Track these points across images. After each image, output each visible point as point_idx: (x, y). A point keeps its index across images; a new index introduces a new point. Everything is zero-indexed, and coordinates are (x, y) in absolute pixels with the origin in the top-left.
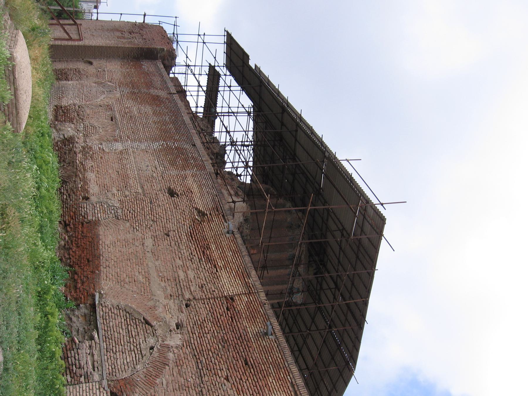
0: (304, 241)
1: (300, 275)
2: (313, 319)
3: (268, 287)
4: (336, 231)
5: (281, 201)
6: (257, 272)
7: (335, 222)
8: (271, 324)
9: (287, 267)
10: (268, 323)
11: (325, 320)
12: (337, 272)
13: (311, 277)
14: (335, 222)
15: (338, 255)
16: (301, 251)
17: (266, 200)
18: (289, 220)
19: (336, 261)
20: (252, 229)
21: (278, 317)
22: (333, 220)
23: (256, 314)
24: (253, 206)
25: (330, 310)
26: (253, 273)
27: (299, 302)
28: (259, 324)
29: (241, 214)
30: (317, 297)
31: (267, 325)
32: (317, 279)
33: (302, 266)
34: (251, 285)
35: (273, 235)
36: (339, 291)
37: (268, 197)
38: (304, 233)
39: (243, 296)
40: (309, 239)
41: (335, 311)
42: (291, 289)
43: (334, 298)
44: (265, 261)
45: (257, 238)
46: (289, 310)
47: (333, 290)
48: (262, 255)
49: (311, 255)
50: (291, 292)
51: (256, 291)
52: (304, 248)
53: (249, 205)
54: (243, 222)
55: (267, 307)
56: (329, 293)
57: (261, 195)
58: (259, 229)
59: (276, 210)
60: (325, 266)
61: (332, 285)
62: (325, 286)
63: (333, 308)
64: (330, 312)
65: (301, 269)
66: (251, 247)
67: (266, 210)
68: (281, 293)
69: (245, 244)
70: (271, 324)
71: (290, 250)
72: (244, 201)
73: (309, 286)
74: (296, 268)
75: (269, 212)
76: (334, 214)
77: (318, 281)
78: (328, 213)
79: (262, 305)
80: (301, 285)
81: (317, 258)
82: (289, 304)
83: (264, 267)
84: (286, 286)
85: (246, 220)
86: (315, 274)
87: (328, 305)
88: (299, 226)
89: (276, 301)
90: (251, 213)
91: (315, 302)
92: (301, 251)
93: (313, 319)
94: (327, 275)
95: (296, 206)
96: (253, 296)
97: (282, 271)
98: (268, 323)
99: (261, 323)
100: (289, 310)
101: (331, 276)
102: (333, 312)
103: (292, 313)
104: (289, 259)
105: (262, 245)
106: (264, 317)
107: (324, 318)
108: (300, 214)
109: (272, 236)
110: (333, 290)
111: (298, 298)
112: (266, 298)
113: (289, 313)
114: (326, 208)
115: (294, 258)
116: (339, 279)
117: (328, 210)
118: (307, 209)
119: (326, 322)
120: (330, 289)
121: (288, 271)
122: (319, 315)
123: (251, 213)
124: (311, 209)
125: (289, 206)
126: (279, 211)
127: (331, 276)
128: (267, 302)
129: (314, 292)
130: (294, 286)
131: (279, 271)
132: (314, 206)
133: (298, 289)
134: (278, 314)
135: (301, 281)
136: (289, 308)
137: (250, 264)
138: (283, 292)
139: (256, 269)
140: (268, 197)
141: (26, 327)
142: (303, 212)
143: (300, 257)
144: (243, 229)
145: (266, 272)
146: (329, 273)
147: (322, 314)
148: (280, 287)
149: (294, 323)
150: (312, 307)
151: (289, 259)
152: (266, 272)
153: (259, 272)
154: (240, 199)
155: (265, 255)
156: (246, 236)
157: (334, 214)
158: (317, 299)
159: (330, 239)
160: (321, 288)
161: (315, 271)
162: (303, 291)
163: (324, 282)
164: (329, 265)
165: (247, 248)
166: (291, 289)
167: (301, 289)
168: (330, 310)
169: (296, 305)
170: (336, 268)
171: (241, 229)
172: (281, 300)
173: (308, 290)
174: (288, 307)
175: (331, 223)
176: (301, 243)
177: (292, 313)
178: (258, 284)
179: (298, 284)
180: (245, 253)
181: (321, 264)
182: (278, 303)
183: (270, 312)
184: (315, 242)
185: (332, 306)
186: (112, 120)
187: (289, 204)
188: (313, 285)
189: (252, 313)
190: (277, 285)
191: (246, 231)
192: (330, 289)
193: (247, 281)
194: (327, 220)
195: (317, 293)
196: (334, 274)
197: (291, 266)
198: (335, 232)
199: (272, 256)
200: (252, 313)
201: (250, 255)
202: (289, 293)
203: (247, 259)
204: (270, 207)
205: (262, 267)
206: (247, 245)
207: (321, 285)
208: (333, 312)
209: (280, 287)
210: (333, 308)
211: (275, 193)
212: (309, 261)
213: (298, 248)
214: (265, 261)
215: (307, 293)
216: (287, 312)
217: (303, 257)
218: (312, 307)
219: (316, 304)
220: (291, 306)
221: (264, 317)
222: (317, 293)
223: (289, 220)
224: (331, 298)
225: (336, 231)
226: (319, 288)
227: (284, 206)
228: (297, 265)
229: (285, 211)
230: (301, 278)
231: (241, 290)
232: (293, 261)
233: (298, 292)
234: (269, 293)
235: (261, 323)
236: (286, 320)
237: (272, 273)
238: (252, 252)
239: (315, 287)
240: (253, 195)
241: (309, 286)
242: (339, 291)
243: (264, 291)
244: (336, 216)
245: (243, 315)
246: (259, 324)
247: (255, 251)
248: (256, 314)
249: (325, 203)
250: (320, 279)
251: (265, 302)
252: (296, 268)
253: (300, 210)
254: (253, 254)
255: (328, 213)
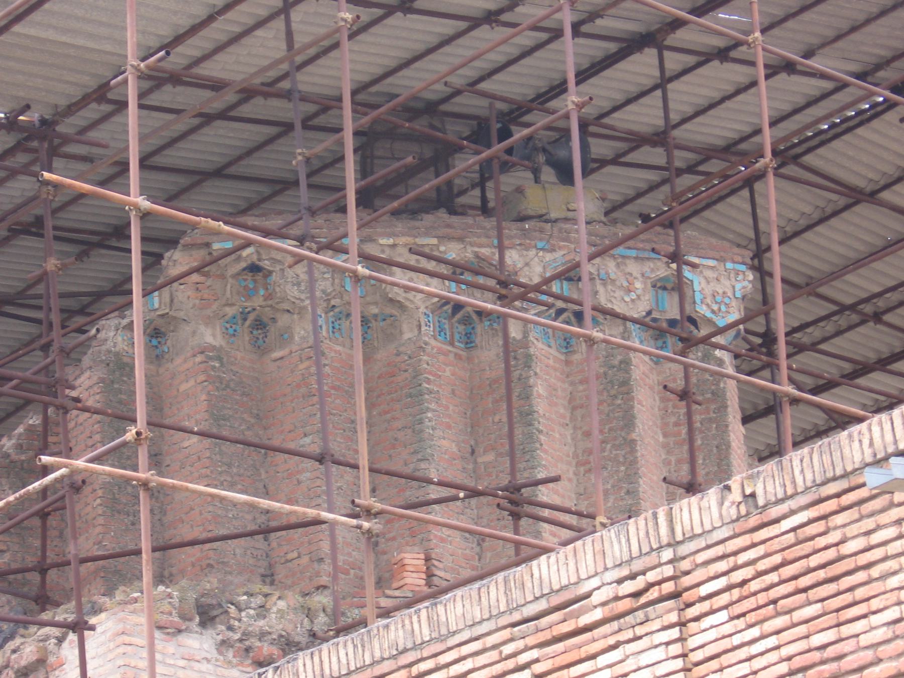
0: (352, 241)
1: (570, 274)
2: (857, 196)
3: (644, 485)
4: (289, 34)
5: (86, 384)
6: (546, 550)
7: (236, 39)
8: (879, 462)
9: (514, 356)
10: (874, 478)
11: (864, 119)
12: (557, 34)
13: (584, 200)
14: (236, 39)
15: (448, 27)
16: (412, 260)
17: (76, 485)
18: (211, 336)
19: (486, 35)
20: (269, 577)
21: (841, 421)
22: (220, 48)
23: (814, 561)
24: (116, 568)
25: (800, 87)
26: (550, 571)
27: (744, 282)
28: (876, 538)
29: (166, 647)
30: (714, 166)
31: (886, 490)
32: (603, 163)
33: (513, 257)
34: (629, 587)
35: (312, 444)
36: (677, 24)
37: (60, 468)
38: (301, 241)
39: (692, 642)
40: (343, 210)
41: (808, 55)
42: (656, 329)
43: (723, 54)
44: (474, 493)
45: (326, 546)
46: (797, 348)
47: (674, 61)
48: (437, 514)
49: (445, 201)
50: (682, 332)
51: (667, 554)
52: (392, 241)
53: (109, 592)
54: (218, 632)
55: (768, 482)
56: (686, 93)
57: (43, 515)
58: (266, 532)
59: (141, 423)
60: (516, 113)
61: (642, 66)
62: (645, 116)
63: (789, 67)
64: (815, 86)
65: (531, 263)
66: (380, 583)
67: (145, 484)
68: (684, 395)
69: (363, 623)
70: (879, 462)
71: (408, 334)
72: (80, 627)
73: (646, 218)
74: (528, 293)
75: (156, 461)
76: (178, 40)
77: (615, 161)
78: (175, 79)
79: (755, 515)
80: (633, 268)
81: (466, 163)
82: (759, 348)
83: (516, 502)
84: (640, 367)
85: (207, 615)
86: (565, 175)
87: (765, 101)
88: (254, 268)
89: (737, 432)
90: (160, 578)
91: (749, 182)
92: (412, 260)
93: (857, 196)
94: (572, 99)
95: (121, 288)
96: (699, 575)
97: (540, 389)
98: (874, 478)
99: (869, 524)
100: (797, 348)
101: (583, 76)
102: (814, 63)
103: (815, 333)
104: (469, 341)
105: (368, 513)
106: (831, 505)
107: (847, 127)
108: (178, 261)
109: (316, 449)
110: (674, 61)
111: (720, 289)
112: (713, 494)
113: (813, 347)
114: (141, 96)
115: (458, 307)
116: (602, 24)
117: (155, 80)
118: (145, 216)
119: (878, 111)
120: (663, 82)
121: (544, 351)
122: (832, 159)
123: (160, 578)
124: (143, 190)
125: (121, 335)
126: (155, 400)
127: (583, 76)
128: (734, 483)
129: (681, 188)
130: (638, 311)
131: (541, 407)
132: (124, 167)
133: (660, 286)
134: (820, 419)
135: (609, 266)
136: (782, 348)
137: (494, 592)
138: (680, 384)
139: (525, 554)
140: (60, 468)
141: (470, 333)
142: (160, 242)
143: (457, 271)
144: (262, 635)
145: (544, 494)
146: (560, 89)
147: (824, 140)
148: (647, 405)
149: (877, 317)
150: (777, 200)
151: (469, 341)
152: (544, 494)
153: (548, 534)
154: (69, 651)
155: (435, 492)
156: (310, 613)
157: (178, 40)
158: (730, 167)
159: (342, 72)
160: (659, 138)
161: (548, 174)
162: (675, 257)
163: (620, 120)
164: (515, 84)
165: (386, 613)
166: (656, 329)
167: (663, 270)
168: (800, 87)
169: (762, 304)
170: (527, 39)
171: (267, 649)
172: (731, 390)
173: (671, 225)
174: (771, 354)
175: (238, 65)
176: (365, 258)
177: (815, 333)
178: (616, 543)
179: (628, 284)
180: (417, 624)
181: (505, 134)
182: (746, 420)
183: (804, 465)
184: (364, 170)
185: (772, 71)
186: (71, 449)
187: (110, 334)
188: (640, 195)
189: (804, 582)
190: (629, 422)
191: (281, 613)
192: (663, 82)
193: (597, 614)
194: (217, 86)
195: (691, 169)
196: (570, 54)
197: (515, 331)
198: (300, 40)
199: (443, 450)
200: (804, 582)
201: (435, 591)
202: (688, 343)
203: (457, 609)
204: (122, 455)
205: (516, 516)
206: (369, 612)
207: (638, 140)
208: (814, 63)
209: (647, 405)
210: (789, 67)
211: (34, 420)
212: (485, 209)
213: (400, 277)
214: (474, 493)
215: (688, 233)
216: (807, 359)
217: (453, 251)
218: (777, 200)
219: (761, 175)
220: (769, 338)
221: (831, 505)
222: (691, 169)
223: (211, 336)
224: (719, 77)
225: (289, 34)
226: (655, 155)
227: (121, 367)
228: (507, 288)
229: (156, 357)
230: (588, 268)
231: (660, 654)
232: (481, 313)
233: (679, 287)
234: (684, 474)
235: (869, 524)
236: (863, 369)
237: (554, 451)
238: (414, 580)
239: (653, 176)
240: (43, 572)
241: (646, 218)
242: (677, 24)
243: (671, 499)
244: (193, 30)
245: (818, 640)
246: (876, 538)
247: (413, 559)
248: (814, 561)
249: (104, 97)
250: (601, 148)
251: (736, 495)
252: (528, 293)
253: (152, 260)
254: (430, 575)
255: (175, 79)
